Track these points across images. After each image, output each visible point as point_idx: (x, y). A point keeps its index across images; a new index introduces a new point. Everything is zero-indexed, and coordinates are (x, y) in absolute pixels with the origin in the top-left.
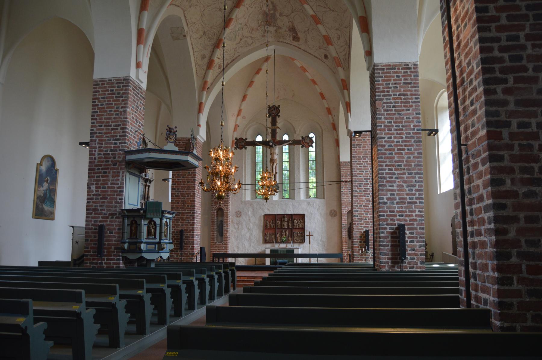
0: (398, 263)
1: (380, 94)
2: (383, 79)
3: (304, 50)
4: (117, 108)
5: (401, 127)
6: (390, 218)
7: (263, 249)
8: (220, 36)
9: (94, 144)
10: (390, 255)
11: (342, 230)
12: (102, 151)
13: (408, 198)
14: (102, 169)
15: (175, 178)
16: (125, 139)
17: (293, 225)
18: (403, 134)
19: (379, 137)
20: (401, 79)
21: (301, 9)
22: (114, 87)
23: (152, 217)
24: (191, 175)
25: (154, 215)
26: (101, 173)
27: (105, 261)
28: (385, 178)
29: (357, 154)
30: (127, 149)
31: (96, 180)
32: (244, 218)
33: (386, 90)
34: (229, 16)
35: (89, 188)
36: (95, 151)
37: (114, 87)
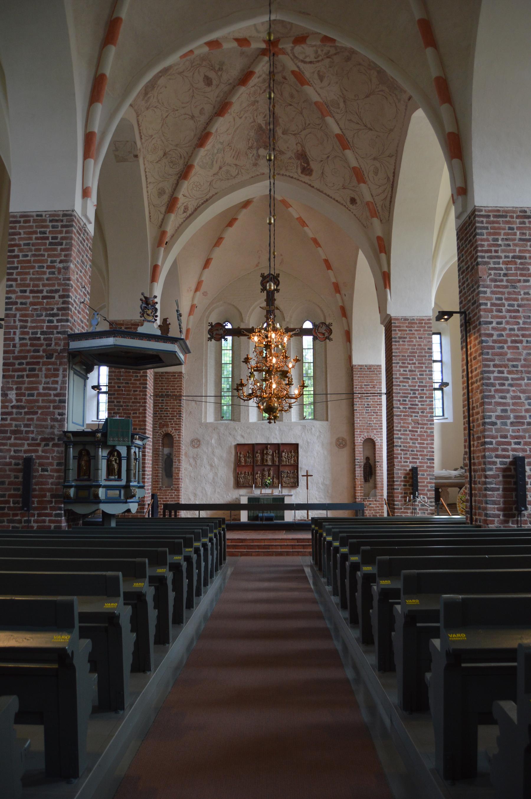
0: (513, 516)
1: (483, 254)
2: (488, 231)
3: (318, 190)
4: (52, 262)
5: (516, 308)
6: (502, 447)
7: (237, 496)
8: (189, 160)
9: (12, 322)
10: (501, 504)
11: (355, 468)
12: (28, 333)
13: (528, 416)
14: (28, 364)
15: (113, 385)
16: (67, 315)
17: (280, 460)
18: (519, 317)
19: (483, 321)
20: (516, 233)
21: (319, 124)
22: (47, 227)
23: (114, 444)
24: (139, 380)
25: (119, 441)
26: (26, 371)
27: (36, 518)
28: (493, 385)
29: (399, 352)
30: (70, 332)
31: (17, 383)
32: (205, 449)
33: (493, 249)
34: (205, 128)
35: (5, 395)
36: (15, 333)
37: (47, 227)
